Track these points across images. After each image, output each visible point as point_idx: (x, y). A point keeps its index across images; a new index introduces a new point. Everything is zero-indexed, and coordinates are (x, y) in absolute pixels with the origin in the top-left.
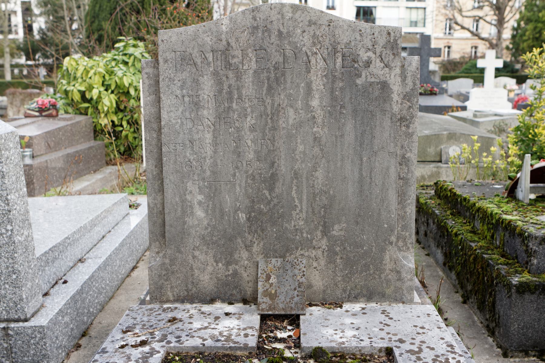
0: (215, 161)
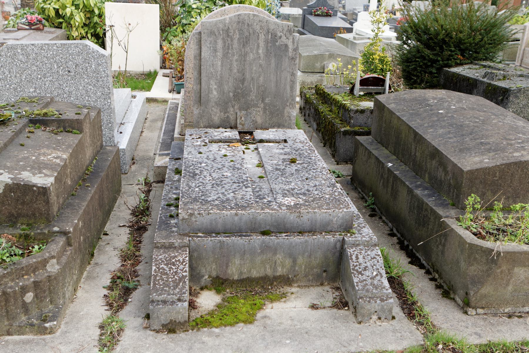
0: (222, 72)
